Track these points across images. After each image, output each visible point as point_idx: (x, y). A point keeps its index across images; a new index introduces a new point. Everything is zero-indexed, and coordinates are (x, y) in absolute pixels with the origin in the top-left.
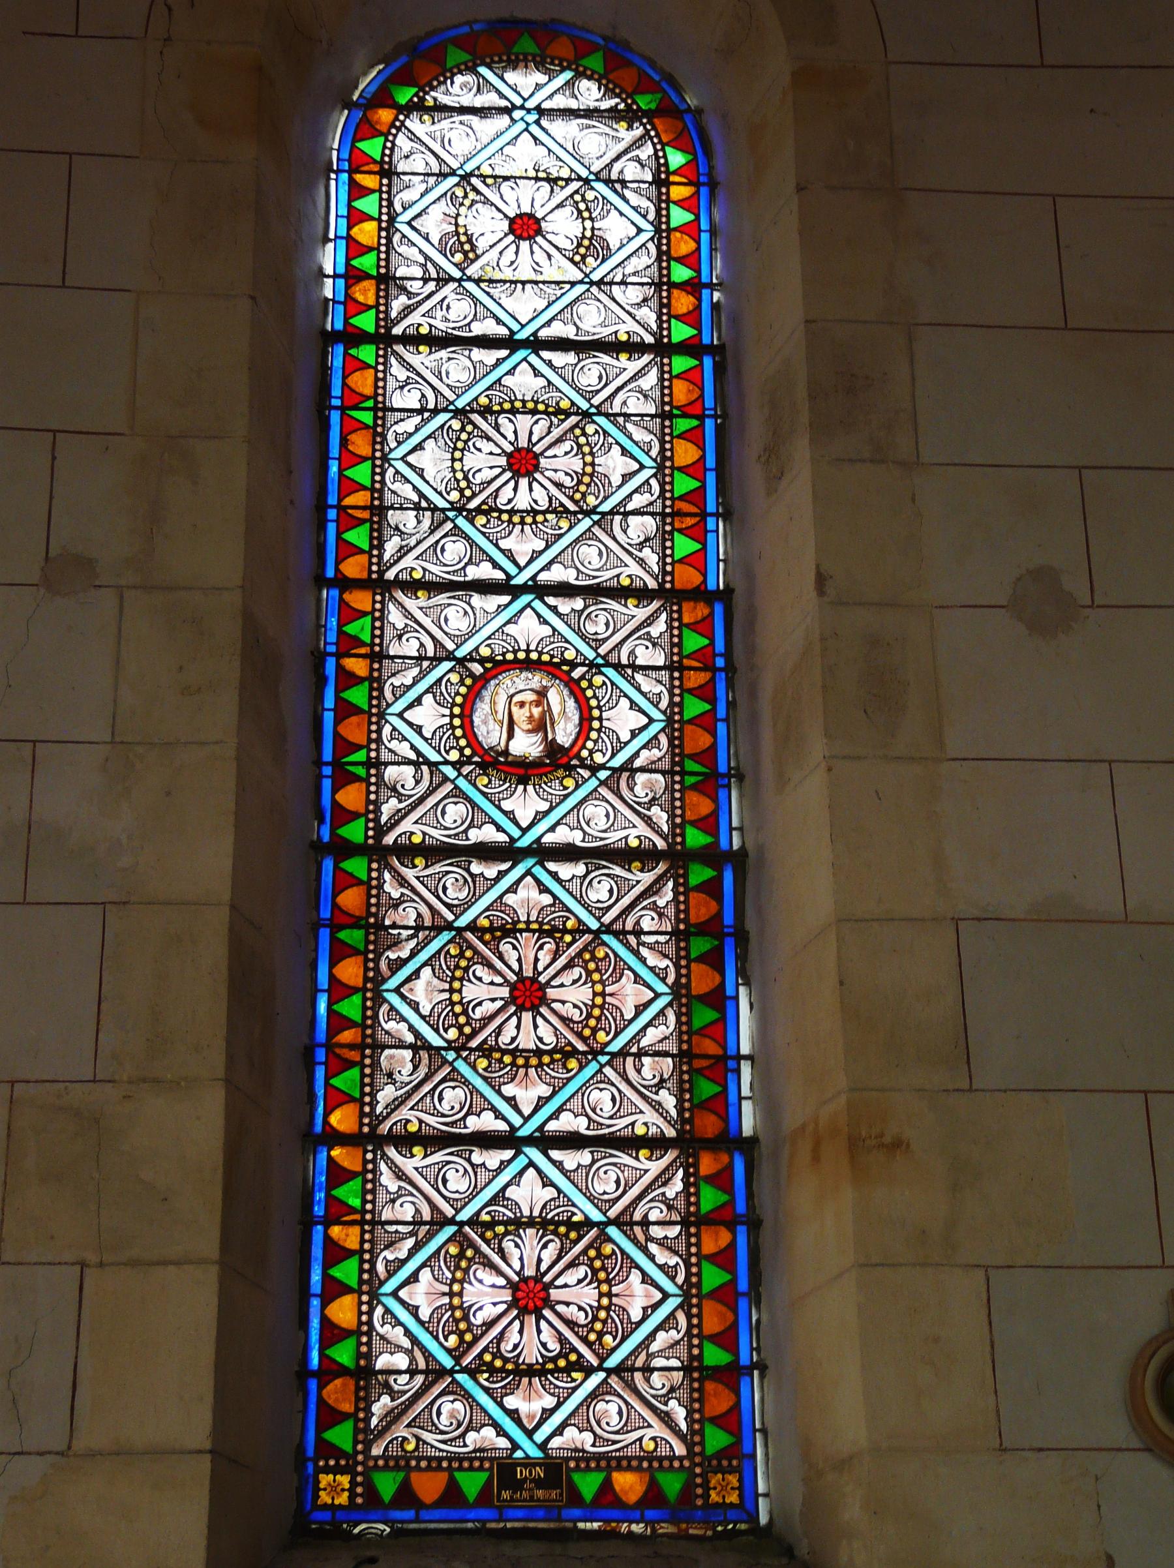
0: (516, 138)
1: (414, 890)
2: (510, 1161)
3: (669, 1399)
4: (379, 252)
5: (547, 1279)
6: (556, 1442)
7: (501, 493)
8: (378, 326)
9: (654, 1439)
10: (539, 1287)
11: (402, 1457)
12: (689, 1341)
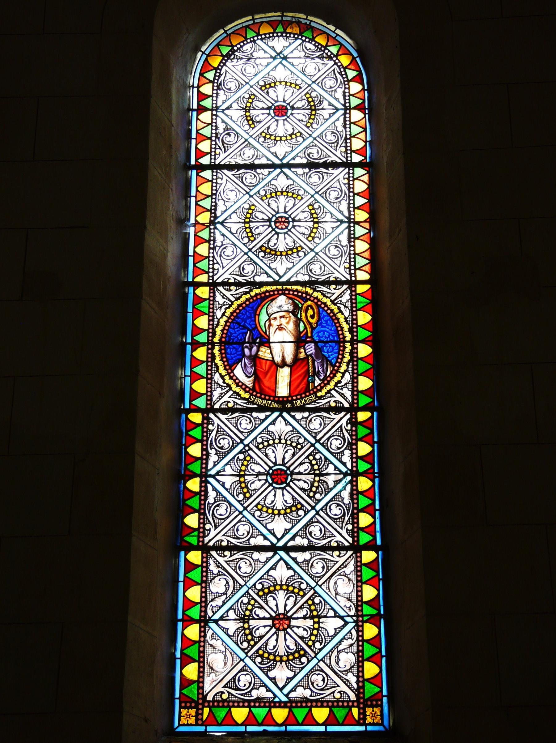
0: (276, 67)
1: (224, 569)
2: (271, 558)
3: (348, 672)
4: (212, 126)
5: (289, 614)
6: (292, 695)
7: (267, 497)
8: (207, 404)
9: (340, 692)
10: (285, 626)
11: (221, 701)
12: (358, 644)
